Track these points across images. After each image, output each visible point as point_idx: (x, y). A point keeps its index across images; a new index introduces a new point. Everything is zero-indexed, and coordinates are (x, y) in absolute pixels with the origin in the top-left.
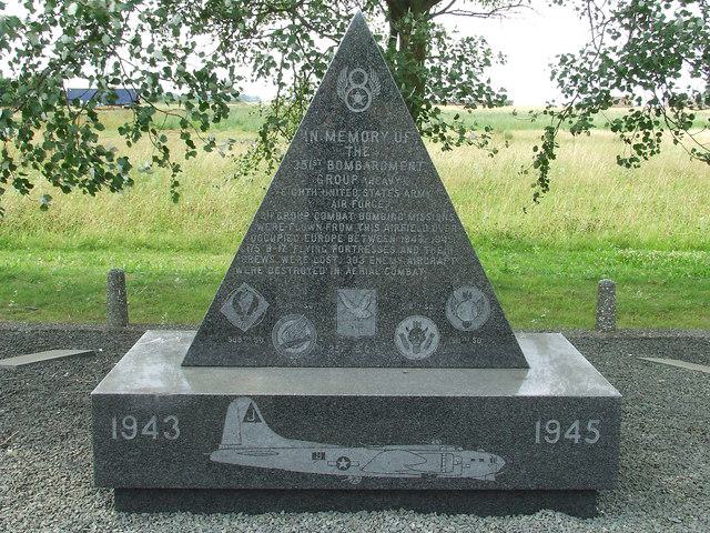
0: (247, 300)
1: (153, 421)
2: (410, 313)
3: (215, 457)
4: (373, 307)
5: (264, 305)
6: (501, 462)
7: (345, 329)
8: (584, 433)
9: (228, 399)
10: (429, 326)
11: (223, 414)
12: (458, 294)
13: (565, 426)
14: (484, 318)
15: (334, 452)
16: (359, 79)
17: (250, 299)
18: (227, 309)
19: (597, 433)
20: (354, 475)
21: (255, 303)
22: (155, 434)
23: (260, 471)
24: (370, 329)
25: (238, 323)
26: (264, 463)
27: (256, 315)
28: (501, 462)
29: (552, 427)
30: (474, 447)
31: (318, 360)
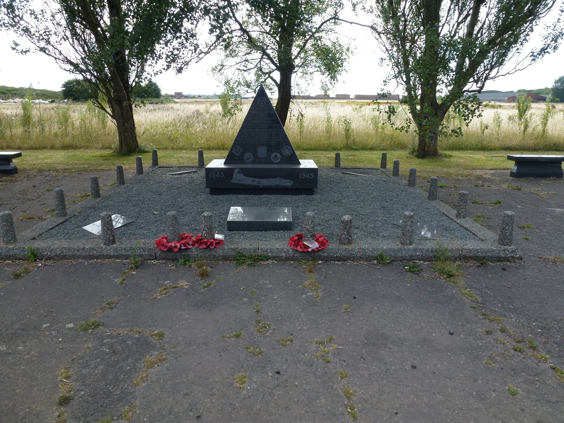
1: (218, 173)
2: (274, 152)
3: (232, 181)
4: (266, 151)
5: (242, 150)
6: (292, 182)
7: (260, 155)
8: (310, 176)
9: (234, 169)
10: (279, 155)
11: (233, 172)
12: (285, 147)
14: (290, 153)
15: (257, 180)
16: (262, 99)
17: (238, 149)
20: (261, 185)
21: (240, 150)
22: (219, 176)
23: (241, 184)
24: (265, 156)
27: (240, 152)
28: (292, 182)
29: (303, 174)
30: (286, 179)
31: (254, 162)
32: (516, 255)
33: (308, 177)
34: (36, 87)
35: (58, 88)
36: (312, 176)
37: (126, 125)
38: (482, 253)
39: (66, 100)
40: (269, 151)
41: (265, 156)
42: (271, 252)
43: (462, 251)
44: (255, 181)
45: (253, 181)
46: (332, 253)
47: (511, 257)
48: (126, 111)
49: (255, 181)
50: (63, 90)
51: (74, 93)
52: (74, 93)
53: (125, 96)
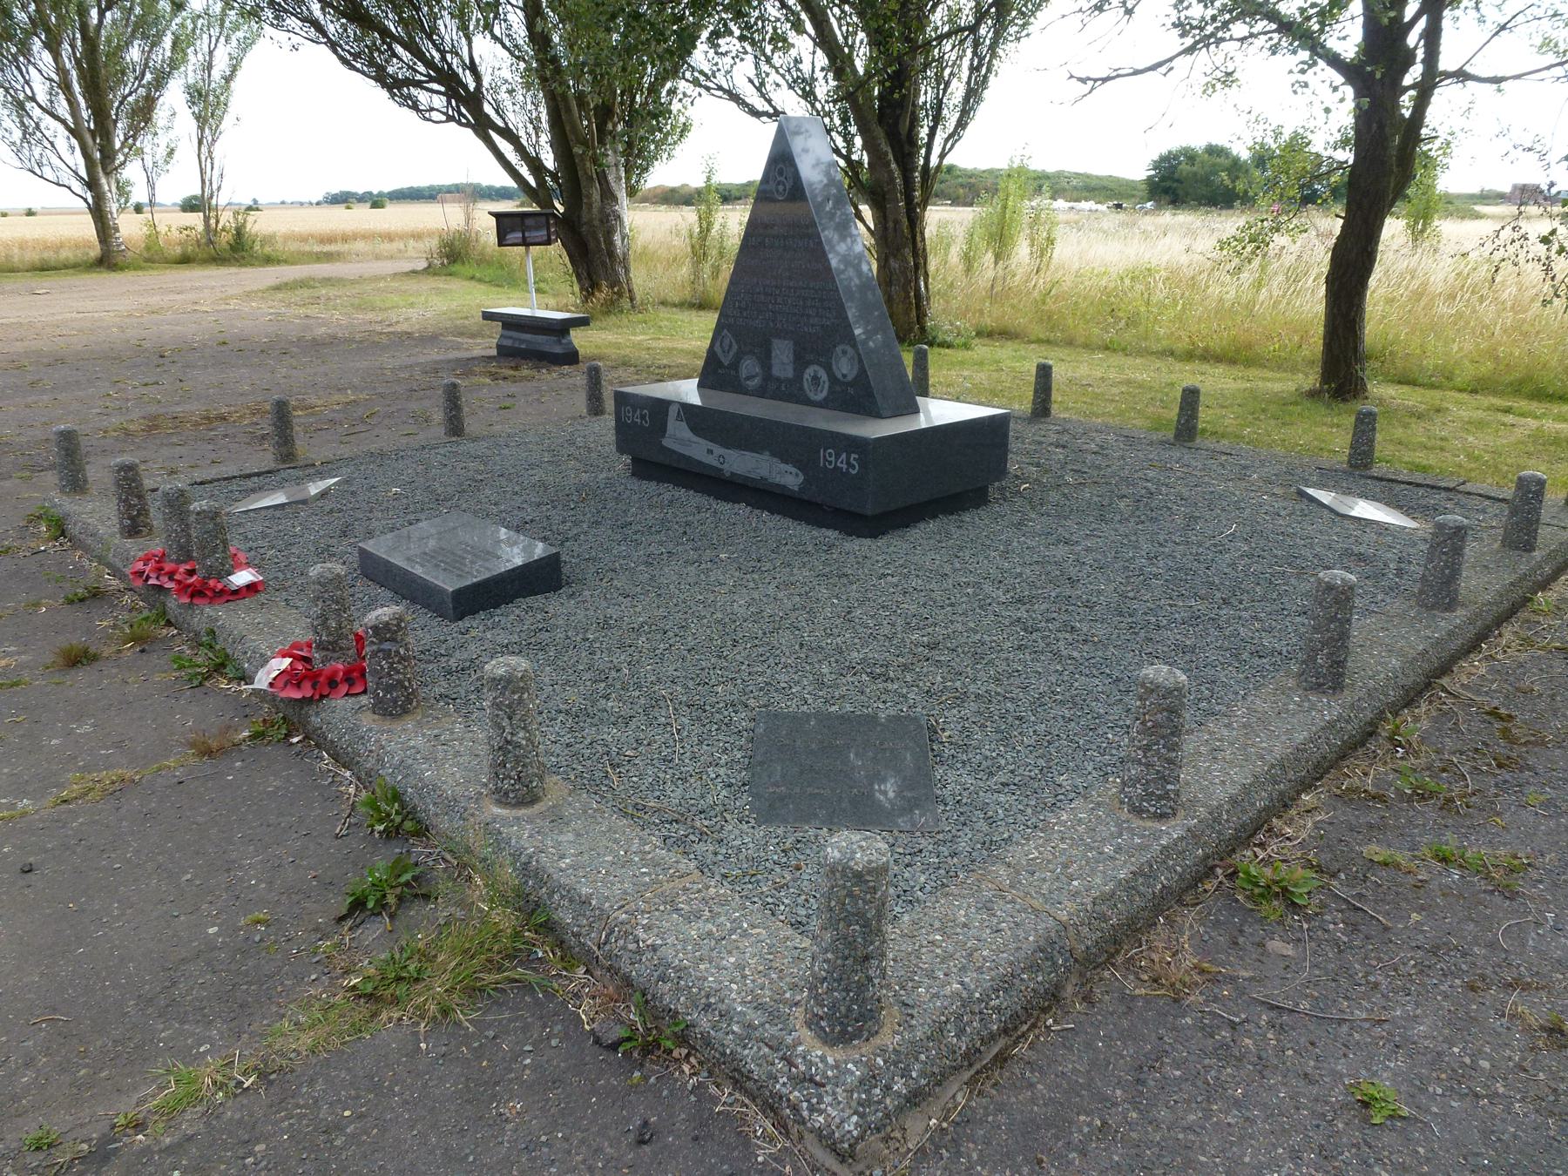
0: (727, 342)
12: (839, 349)
13: (838, 456)
14: (855, 372)
15: (718, 450)
18: (717, 349)
21: (730, 346)
24: (790, 373)
27: (731, 353)
31: (761, 393)
32: (812, 1109)
34: (1038, 164)
35: (1138, 170)
36: (854, 468)
39: (1149, 205)
40: (801, 362)
41: (790, 373)
50: (1150, 178)
51: (1175, 185)
52: (1175, 185)
53: (892, 179)
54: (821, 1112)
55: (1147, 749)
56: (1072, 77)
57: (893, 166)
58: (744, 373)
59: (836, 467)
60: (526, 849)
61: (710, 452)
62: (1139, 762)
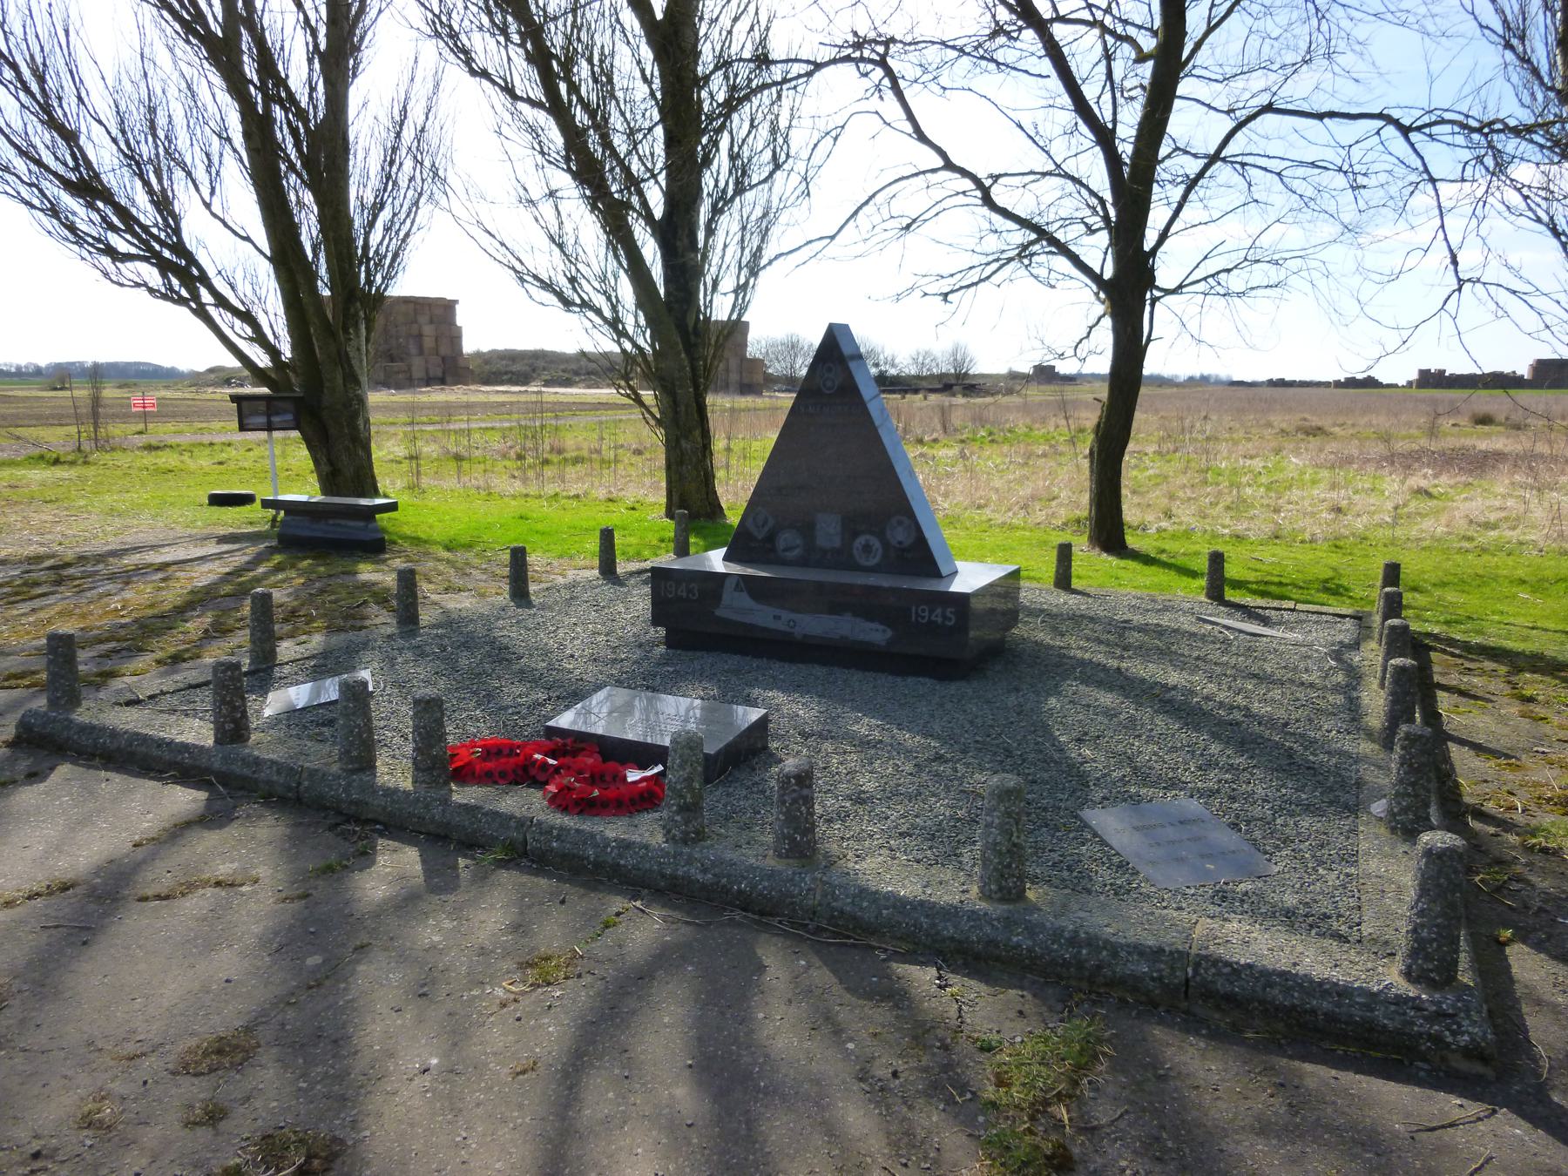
3: (718, 612)
6: (889, 633)
7: (822, 542)
8: (945, 617)
10: (876, 543)
11: (722, 586)
13: (931, 611)
15: (786, 615)
19: (952, 616)
20: (798, 632)
22: (684, 595)
23: (744, 624)
24: (837, 543)
25: (756, 533)
26: (747, 619)
27: (766, 529)
28: (889, 633)
29: (923, 611)
30: (872, 620)
31: (803, 562)
32: (1454, 1033)
33: (940, 620)
37: (684, 443)
38: (1287, 991)
41: (837, 543)
42: (558, 838)
43: (1197, 965)
44: (779, 618)
45: (775, 617)
46: (729, 876)
47: (1430, 1037)
48: (683, 408)
49: (779, 618)
54: (1463, 1034)
55: (1413, 784)
56: (926, 294)
57: (683, 355)
58: (781, 543)
59: (930, 622)
60: (1066, 927)
61: (777, 618)
62: (1409, 795)
